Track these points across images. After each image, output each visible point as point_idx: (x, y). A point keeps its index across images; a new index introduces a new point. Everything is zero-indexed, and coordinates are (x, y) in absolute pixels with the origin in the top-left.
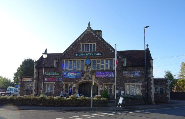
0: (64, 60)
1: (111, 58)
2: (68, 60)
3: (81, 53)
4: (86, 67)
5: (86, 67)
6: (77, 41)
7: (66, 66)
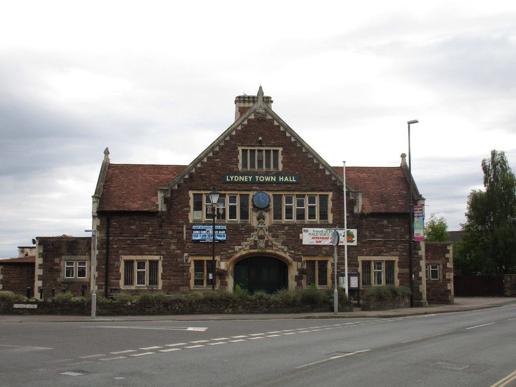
0: (191, 193)
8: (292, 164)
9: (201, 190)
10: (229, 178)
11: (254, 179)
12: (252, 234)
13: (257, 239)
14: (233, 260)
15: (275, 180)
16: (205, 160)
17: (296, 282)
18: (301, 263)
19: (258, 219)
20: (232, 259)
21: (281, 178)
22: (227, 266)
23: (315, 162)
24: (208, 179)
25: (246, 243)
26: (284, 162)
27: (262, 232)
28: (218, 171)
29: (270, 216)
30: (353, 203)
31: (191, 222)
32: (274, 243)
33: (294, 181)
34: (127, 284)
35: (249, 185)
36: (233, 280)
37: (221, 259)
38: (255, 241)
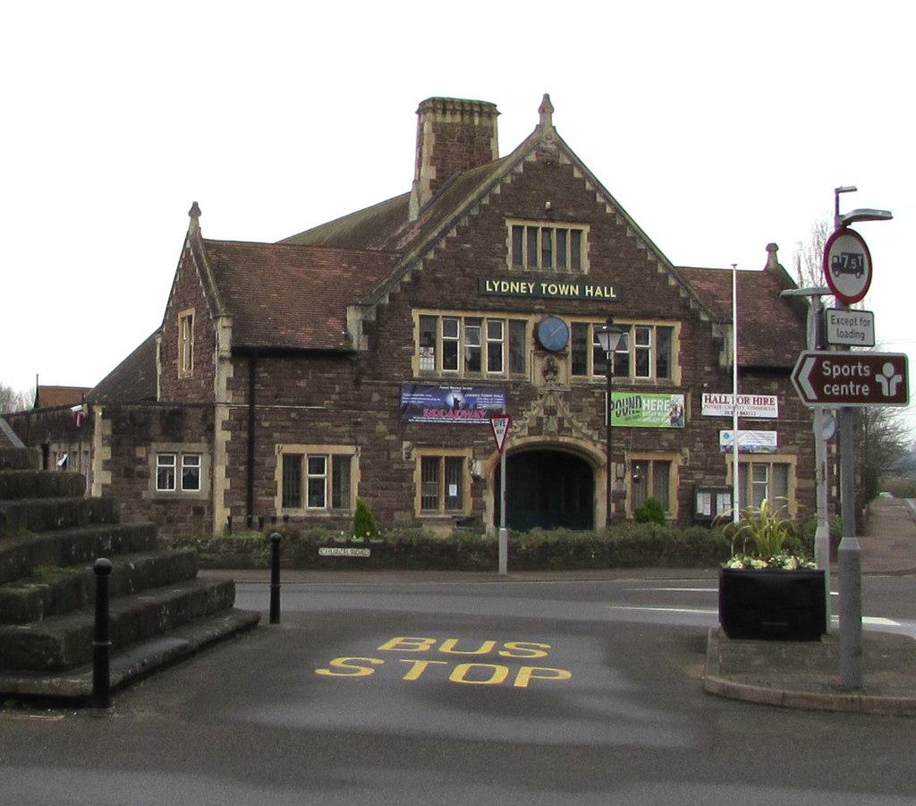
1: (663, 318)
8: (608, 262)
10: (492, 286)
13: (542, 414)
19: (545, 373)
25: (521, 422)
37: (474, 455)
38: (540, 419)
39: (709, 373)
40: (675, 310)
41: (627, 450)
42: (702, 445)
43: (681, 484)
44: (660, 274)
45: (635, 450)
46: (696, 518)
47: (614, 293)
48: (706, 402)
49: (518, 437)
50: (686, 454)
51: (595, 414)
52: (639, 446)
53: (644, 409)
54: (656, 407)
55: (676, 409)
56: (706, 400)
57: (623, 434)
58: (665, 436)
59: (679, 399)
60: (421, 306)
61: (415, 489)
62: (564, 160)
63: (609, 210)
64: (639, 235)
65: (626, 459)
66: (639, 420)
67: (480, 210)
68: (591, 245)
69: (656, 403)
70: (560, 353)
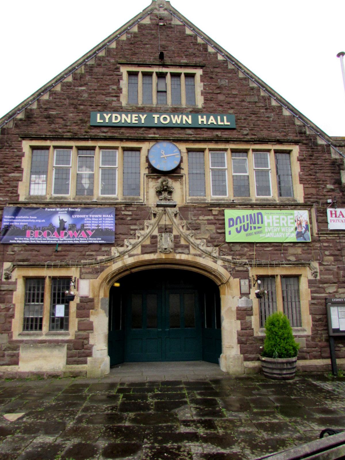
1: (279, 142)
2: (48, 143)
3: (127, 111)
4: (153, 185)
5: (153, 185)
6: (102, 54)
7: (32, 173)
8: (221, 97)
9: (45, 139)
10: (102, 118)
11: (150, 118)
12: (146, 223)
13: (156, 233)
14: (107, 277)
15: (190, 122)
16: (58, 88)
17: (239, 322)
18: (247, 281)
19: (159, 193)
20: (103, 275)
21: (202, 118)
22: (92, 288)
23: (262, 94)
24: (61, 121)
25: (133, 241)
26: (206, 93)
27: (167, 218)
28: (82, 107)
29: (182, 188)
30: (339, 166)
31: (22, 199)
32: (192, 240)
33: (226, 123)
34: (309, 283)
35: (141, 131)
36: (106, 320)
37: (81, 273)
38: (154, 237)
39: (332, 190)
40: (291, 137)
41: (251, 265)
42: (332, 258)
43: (313, 298)
44: (274, 107)
45: (260, 265)
46: (332, 334)
47: (227, 122)
48: (331, 216)
49: (130, 256)
50: (316, 268)
51: (214, 231)
52: (264, 262)
53: (266, 225)
54: (279, 223)
55: (300, 224)
56: (331, 214)
57: (246, 249)
58: (291, 251)
59: (303, 215)
60: (32, 139)
61: (14, 310)
62: (176, 22)
63: (220, 58)
64: (250, 76)
65: (250, 275)
66: (261, 235)
67: (96, 61)
68: (204, 85)
69: (279, 219)
70: (282, 227)
